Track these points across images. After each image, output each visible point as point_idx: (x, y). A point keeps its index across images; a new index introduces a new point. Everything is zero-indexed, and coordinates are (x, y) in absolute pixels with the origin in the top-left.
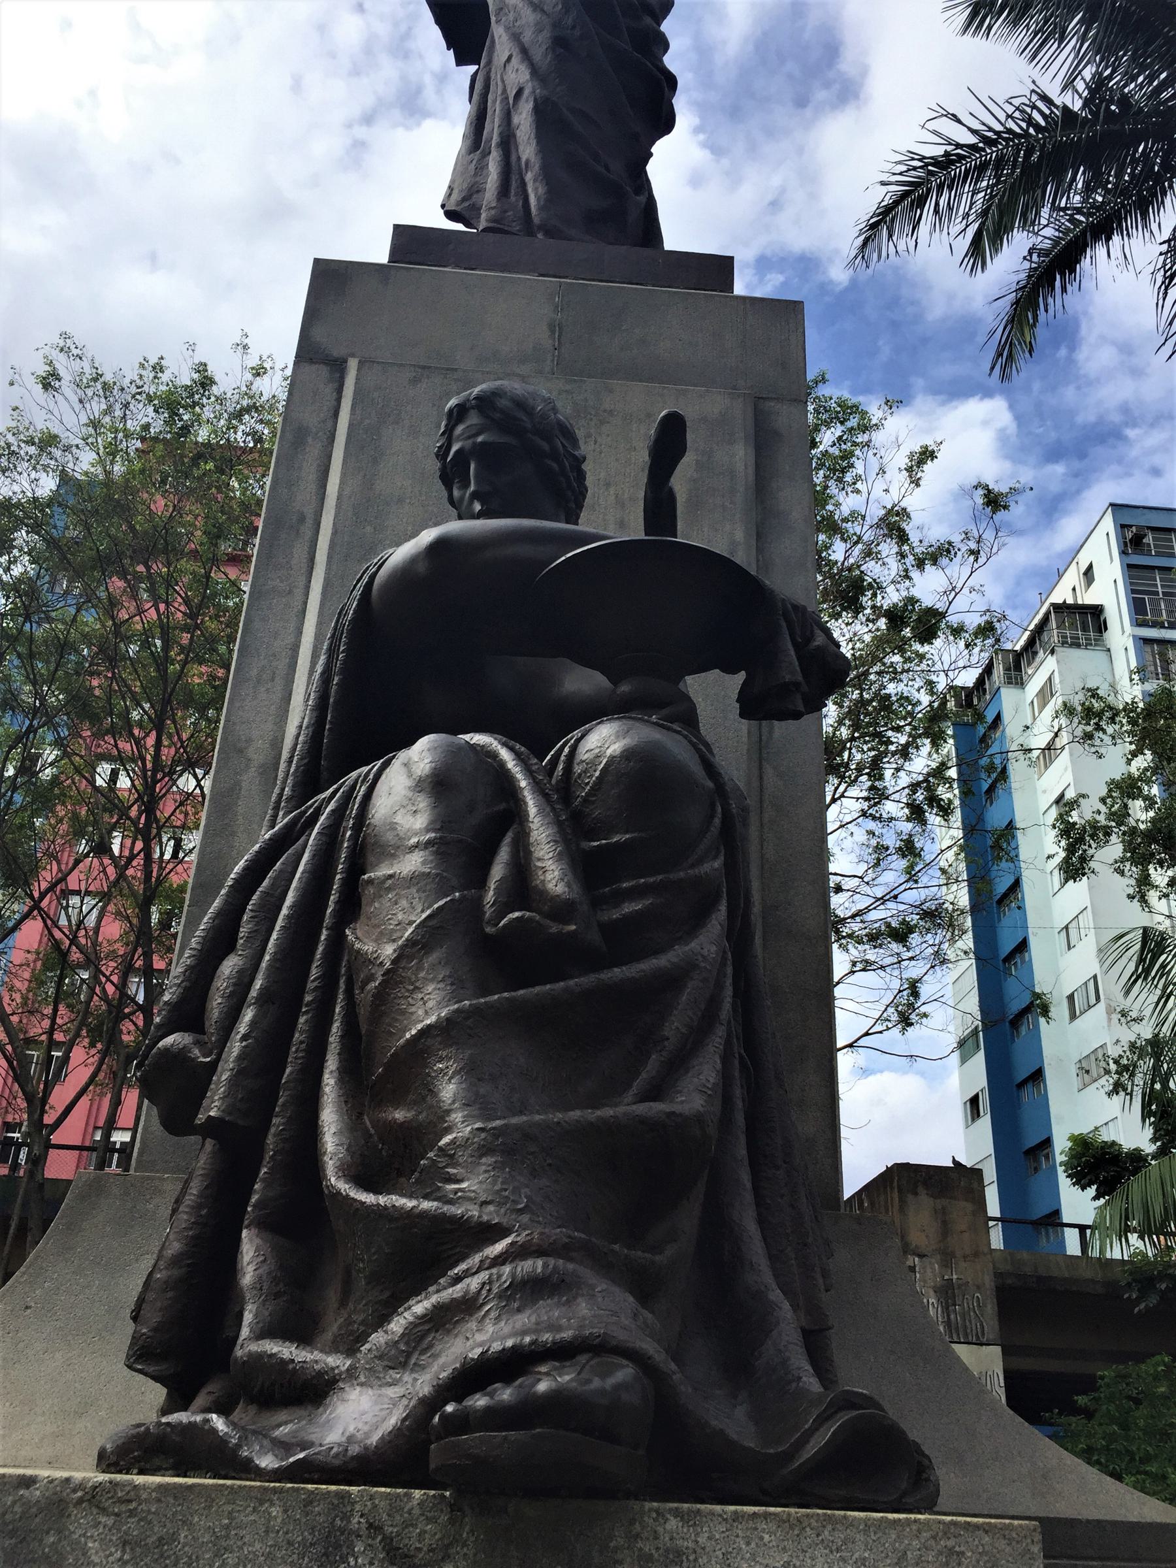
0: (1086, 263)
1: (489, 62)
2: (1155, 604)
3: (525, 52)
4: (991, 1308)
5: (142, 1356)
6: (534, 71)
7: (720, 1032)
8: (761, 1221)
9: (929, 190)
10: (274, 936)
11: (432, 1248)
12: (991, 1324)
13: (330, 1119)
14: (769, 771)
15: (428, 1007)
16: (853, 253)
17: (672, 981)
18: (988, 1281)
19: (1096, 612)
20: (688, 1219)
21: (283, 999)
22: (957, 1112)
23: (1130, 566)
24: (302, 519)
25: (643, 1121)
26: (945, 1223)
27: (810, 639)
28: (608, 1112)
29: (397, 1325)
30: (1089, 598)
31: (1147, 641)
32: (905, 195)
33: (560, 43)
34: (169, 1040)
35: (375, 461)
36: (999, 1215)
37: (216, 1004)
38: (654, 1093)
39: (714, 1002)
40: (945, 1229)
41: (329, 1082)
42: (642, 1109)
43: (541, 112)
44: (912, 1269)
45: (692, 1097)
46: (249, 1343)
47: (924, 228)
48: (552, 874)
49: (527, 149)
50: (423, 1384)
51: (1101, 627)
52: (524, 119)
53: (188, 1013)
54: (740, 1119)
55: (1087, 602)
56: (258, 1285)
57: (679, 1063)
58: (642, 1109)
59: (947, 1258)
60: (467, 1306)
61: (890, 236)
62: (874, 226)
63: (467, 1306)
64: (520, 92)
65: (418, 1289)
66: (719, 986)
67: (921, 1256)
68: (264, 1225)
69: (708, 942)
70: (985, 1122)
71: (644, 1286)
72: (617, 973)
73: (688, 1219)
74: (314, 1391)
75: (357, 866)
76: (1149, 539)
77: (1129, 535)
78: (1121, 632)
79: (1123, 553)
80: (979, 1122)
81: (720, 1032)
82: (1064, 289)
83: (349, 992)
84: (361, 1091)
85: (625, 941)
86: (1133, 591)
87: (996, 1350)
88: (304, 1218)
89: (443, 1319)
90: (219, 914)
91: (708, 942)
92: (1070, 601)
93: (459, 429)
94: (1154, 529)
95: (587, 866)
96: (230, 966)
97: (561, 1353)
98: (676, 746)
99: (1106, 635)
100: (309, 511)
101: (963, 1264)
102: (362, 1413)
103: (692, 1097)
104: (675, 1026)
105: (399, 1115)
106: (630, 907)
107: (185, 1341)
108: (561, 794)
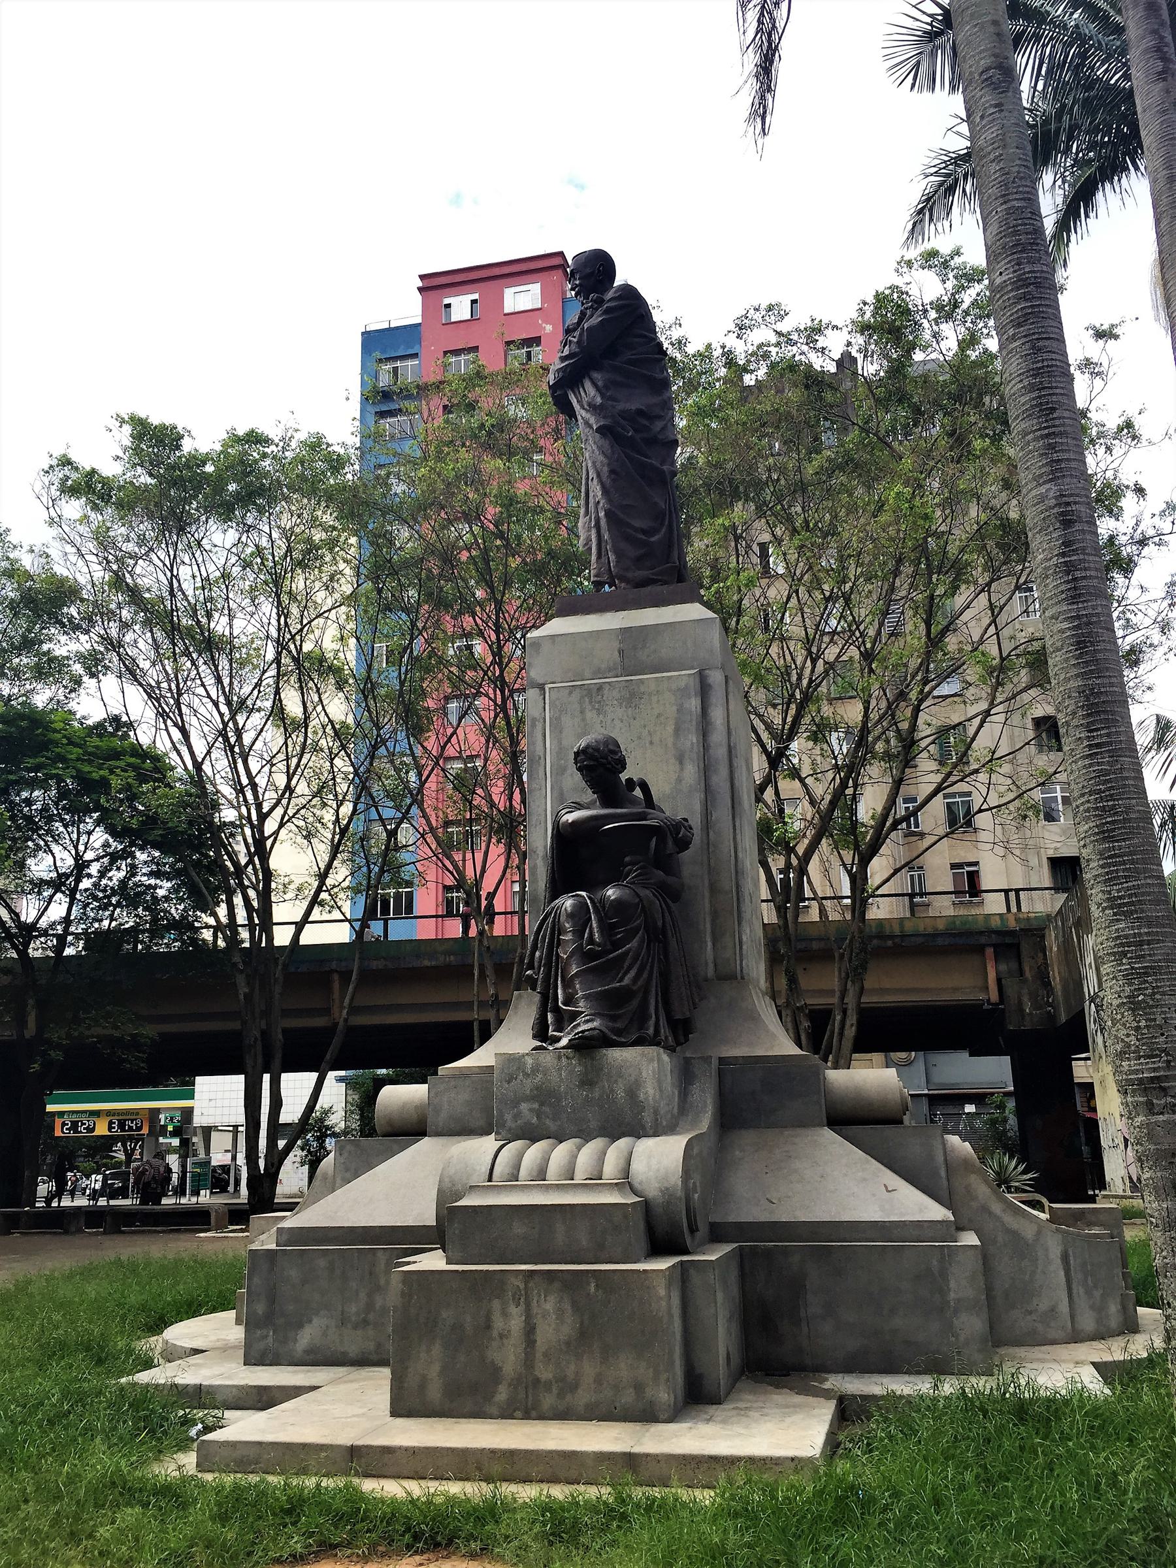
0: (1099, 196)
5: (535, 1037)
9: (956, 180)
10: (415, 1488)
11: (574, 1016)
13: (560, 991)
14: (711, 833)
15: (574, 970)
16: (906, 235)
17: (626, 953)
32: (941, 184)
33: (612, 472)
35: (561, 732)
36: (239, 1081)
37: (536, 964)
43: (608, 514)
46: (550, 1033)
47: (956, 210)
49: (603, 523)
60: (578, 1025)
61: (931, 220)
62: (920, 212)
63: (578, 1025)
74: (558, 1039)
82: (1087, 216)
84: (565, 988)
85: (616, 945)
88: (557, 1010)
89: (575, 1027)
96: (537, 954)
102: (564, 1042)
107: (541, 1032)
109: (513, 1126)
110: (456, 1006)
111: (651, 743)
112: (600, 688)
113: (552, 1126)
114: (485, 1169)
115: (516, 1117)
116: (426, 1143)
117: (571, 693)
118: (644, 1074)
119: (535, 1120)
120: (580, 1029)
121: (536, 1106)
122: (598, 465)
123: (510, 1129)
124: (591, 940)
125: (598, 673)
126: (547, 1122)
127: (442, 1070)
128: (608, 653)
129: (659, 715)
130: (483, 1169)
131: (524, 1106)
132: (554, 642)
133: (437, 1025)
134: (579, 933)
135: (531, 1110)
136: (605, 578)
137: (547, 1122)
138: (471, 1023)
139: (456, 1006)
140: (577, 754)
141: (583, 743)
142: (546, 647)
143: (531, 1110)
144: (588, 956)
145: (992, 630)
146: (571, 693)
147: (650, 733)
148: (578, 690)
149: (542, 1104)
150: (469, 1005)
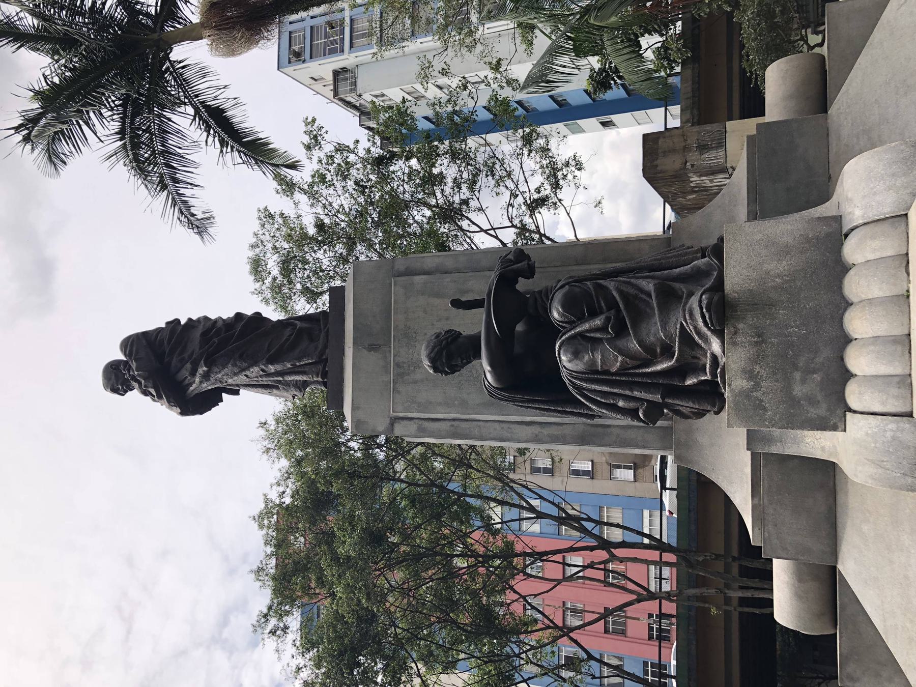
1: (237, 385)
2: (330, 43)
3: (243, 370)
4: (708, 127)
6: (252, 366)
7: (632, 280)
8: (676, 268)
12: (715, 127)
13: (659, 367)
17: (621, 292)
18: (696, 129)
19: (336, 73)
20: (677, 285)
21: (631, 385)
22: (611, 133)
23: (311, 58)
24: (452, 426)
25: (656, 297)
26: (670, 151)
27: (511, 261)
28: (655, 305)
29: (700, 341)
30: (330, 77)
31: (351, 46)
34: (641, 415)
35: (431, 403)
36: (663, 109)
38: (649, 295)
39: (624, 282)
40: (673, 151)
41: (649, 370)
42: (654, 298)
43: (271, 361)
44: (693, 166)
45: (649, 286)
46: (708, 377)
48: (598, 322)
49: (279, 367)
50: (709, 333)
51: (345, 70)
52: (272, 368)
53: (633, 413)
54: (652, 274)
55: (331, 78)
56: (696, 378)
57: (642, 291)
58: (654, 298)
59: (686, 149)
60: (696, 328)
63: (696, 328)
64: (263, 370)
65: (693, 339)
66: (620, 281)
67: (686, 162)
68: (684, 380)
69: (611, 284)
70: (614, 118)
71: (690, 294)
72: (621, 306)
73: (677, 285)
75: (597, 372)
76: (296, 48)
77: (295, 59)
78: (346, 60)
79: (304, 61)
80: (614, 121)
81: (632, 280)
83: (630, 369)
85: (612, 305)
86: (325, 55)
87: (729, 124)
88: (681, 371)
89: (698, 332)
90: (607, 410)
91: (611, 284)
92: (332, 87)
93: (440, 368)
94: (290, 46)
95: (593, 314)
96: (621, 404)
97: (701, 308)
98: (559, 296)
99: (349, 68)
100: (449, 423)
101: (689, 142)
102: (716, 346)
103: (649, 286)
104: (632, 291)
105: (658, 350)
106: (603, 304)
108: (573, 324)
109: (824, 406)
110: (727, 630)
111: (447, 319)
112: (398, 365)
113: (826, 353)
114: (891, 424)
115: (812, 401)
116: (848, 568)
117: (399, 392)
118: (759, 237)
119: (817, 377)
120: (701, 323)
121: (797, 375)
122: (236, 370)
123: (829, 410)
124: (603, 329)
125: (386, 370)
126: (820, 360)
127: (755, 539)
128: (373, 359)
129: (425, 312)
130: (892, 426)
131: (798, 390)
132: (358, 408)
133: (742, 641)
134: (595, 343)
135: (803, 381)
136: (320, 367)
137: (820, 360)
138: (740, 613)
139: (727, 630)
140: (436, 370)
141: (426, 363)
142: (361, 415)
143: (803, 381)
144: (621, 331)
145: (492, 232)
146: (399, 392)
147: (440, 320)
148: (397, 386)
149: (795, 367)
150: (727, 614)
